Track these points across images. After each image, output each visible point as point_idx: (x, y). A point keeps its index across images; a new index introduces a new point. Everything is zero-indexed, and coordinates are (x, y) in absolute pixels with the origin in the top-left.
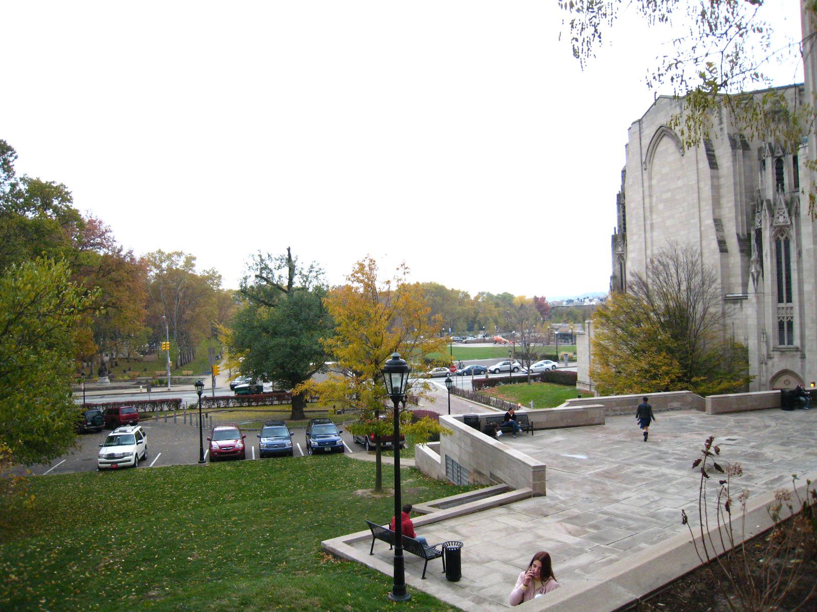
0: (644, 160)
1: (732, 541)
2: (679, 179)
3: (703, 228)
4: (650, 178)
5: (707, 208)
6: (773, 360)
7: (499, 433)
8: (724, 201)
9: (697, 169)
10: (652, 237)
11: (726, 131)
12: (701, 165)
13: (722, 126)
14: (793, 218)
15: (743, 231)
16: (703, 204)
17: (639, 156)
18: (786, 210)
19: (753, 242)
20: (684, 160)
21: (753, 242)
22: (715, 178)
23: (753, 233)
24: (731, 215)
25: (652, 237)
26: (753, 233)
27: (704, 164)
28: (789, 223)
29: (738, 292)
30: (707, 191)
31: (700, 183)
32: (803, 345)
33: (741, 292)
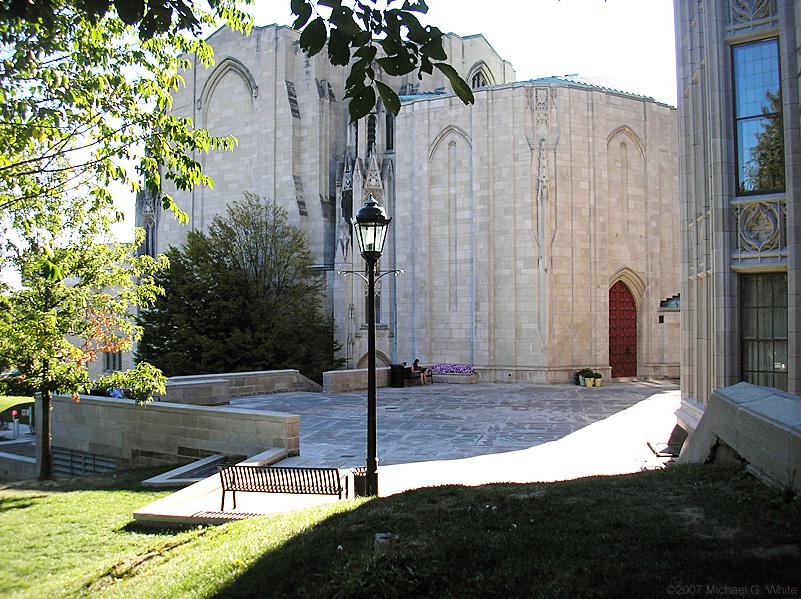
0: (198, 97)
1: (796, 430)
2: (247, 124)
3: (277, 186)
4: (205, 122)
5: (285, 161)
6: (361, 340)
7: (428, 30)
8: (305, 156)
9: (275, 115)
10: (203, 194)
11: (313, 76)
12: (280, 111)
13: (309, 69)
14: (386, 183)
15: (326, 194)
16: (280, 157)
17: (191, 92)
18: (378, 173)
19: (338, 206)
20: (256, 103)
21: (338, 206)
22: (297, 127)
23: (339, 195)
24: (314, 173)
25: (203, 194)
26: (339, 195)
27: (285, 109)
28: (381, 187)
29: (320, 262)
30: (286, 139)
31: (277, 132)
32: (394, 324)
33: (322, 262)
